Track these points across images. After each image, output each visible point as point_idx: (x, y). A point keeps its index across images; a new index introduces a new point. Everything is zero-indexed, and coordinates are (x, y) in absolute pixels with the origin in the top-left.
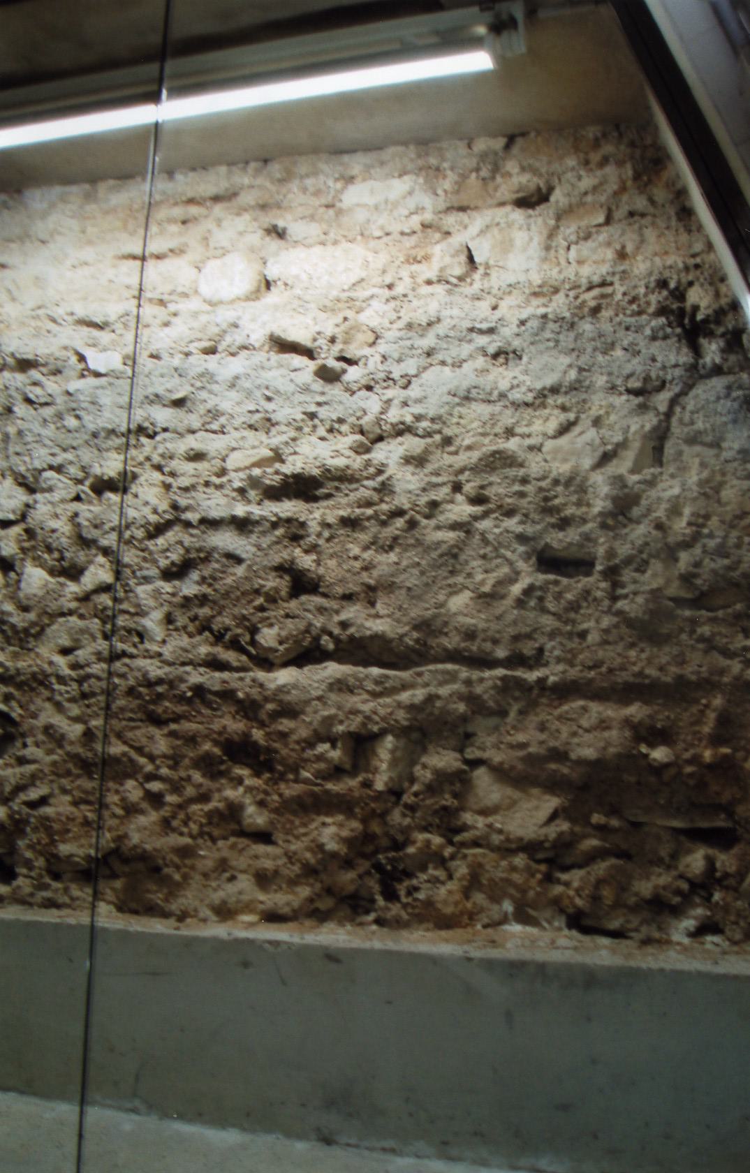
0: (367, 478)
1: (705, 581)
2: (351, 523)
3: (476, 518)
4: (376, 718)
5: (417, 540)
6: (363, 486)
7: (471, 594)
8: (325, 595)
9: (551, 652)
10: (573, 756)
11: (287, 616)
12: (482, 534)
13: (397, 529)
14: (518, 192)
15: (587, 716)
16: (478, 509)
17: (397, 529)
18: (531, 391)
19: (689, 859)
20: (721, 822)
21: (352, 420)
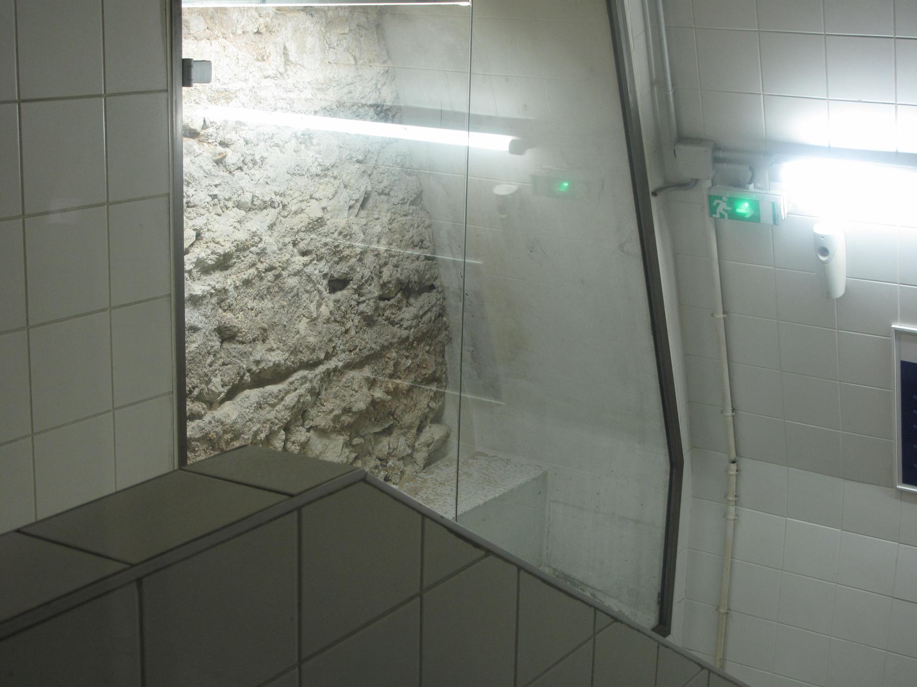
0: (253, 246)
1: (393, 284)
2: (247, 283)
3: (305, 265)
4: (277, 421)
5: (280, 287)
6: (251, 252)
7: (308, 320)
8: (242, 343)
9: (339, 347)
10: (354, 409)
11: (224, 364)
12: (309, 276)
13: (269, 281)
14: (463, 295)
15: (223, 312)
16: (306, 259)
17: (269, 281)
18: (320, 165)
19: (379, 447)
20: (493, 458)
21: (235, 198)
